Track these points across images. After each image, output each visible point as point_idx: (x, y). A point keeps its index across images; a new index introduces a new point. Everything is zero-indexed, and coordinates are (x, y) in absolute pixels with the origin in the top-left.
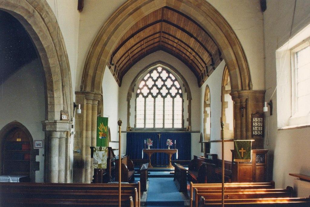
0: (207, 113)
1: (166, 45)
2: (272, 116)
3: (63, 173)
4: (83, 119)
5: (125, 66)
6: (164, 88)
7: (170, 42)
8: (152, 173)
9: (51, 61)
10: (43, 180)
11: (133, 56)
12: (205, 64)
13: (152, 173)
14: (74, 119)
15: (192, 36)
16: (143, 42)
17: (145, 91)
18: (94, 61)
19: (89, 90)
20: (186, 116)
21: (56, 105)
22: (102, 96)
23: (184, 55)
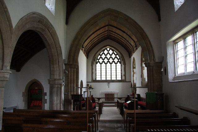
3: (59, 105)
6: (111, 59)
7: (113, 35)
8: (105, 105)
10: (49, 108)
11: (94, 43)
12: (132, 46)
13: (105, 105)
14: (64, 78)
15: (124, 32)
20: (123, 73)
22: (78, 66)
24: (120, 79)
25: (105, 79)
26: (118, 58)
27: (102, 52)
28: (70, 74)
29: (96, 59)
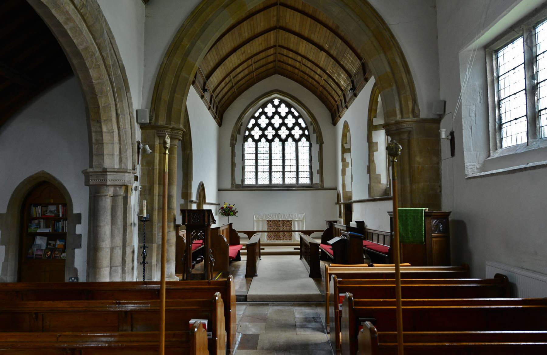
0: (345, 161)
1: (284, 66)
2: (454, 157)
4: (154, 166)
5: (226, 97)
7: (290, 61)
8: (267, 250)
9: (93, 73)
12: (342, 90)
13: (267, 250)
14: (138, 167)
15: (321, 48)
16: (250, 60)
17: (256, 133)
18: (170, 79)
19: (165, 124)
21: (107, 143)
23: (310, 80)
24: (307, 181)
25: (266, 182)
26: (303, 125)
27: (260, 110)
28: (157, 156)
29: (242, 128)
